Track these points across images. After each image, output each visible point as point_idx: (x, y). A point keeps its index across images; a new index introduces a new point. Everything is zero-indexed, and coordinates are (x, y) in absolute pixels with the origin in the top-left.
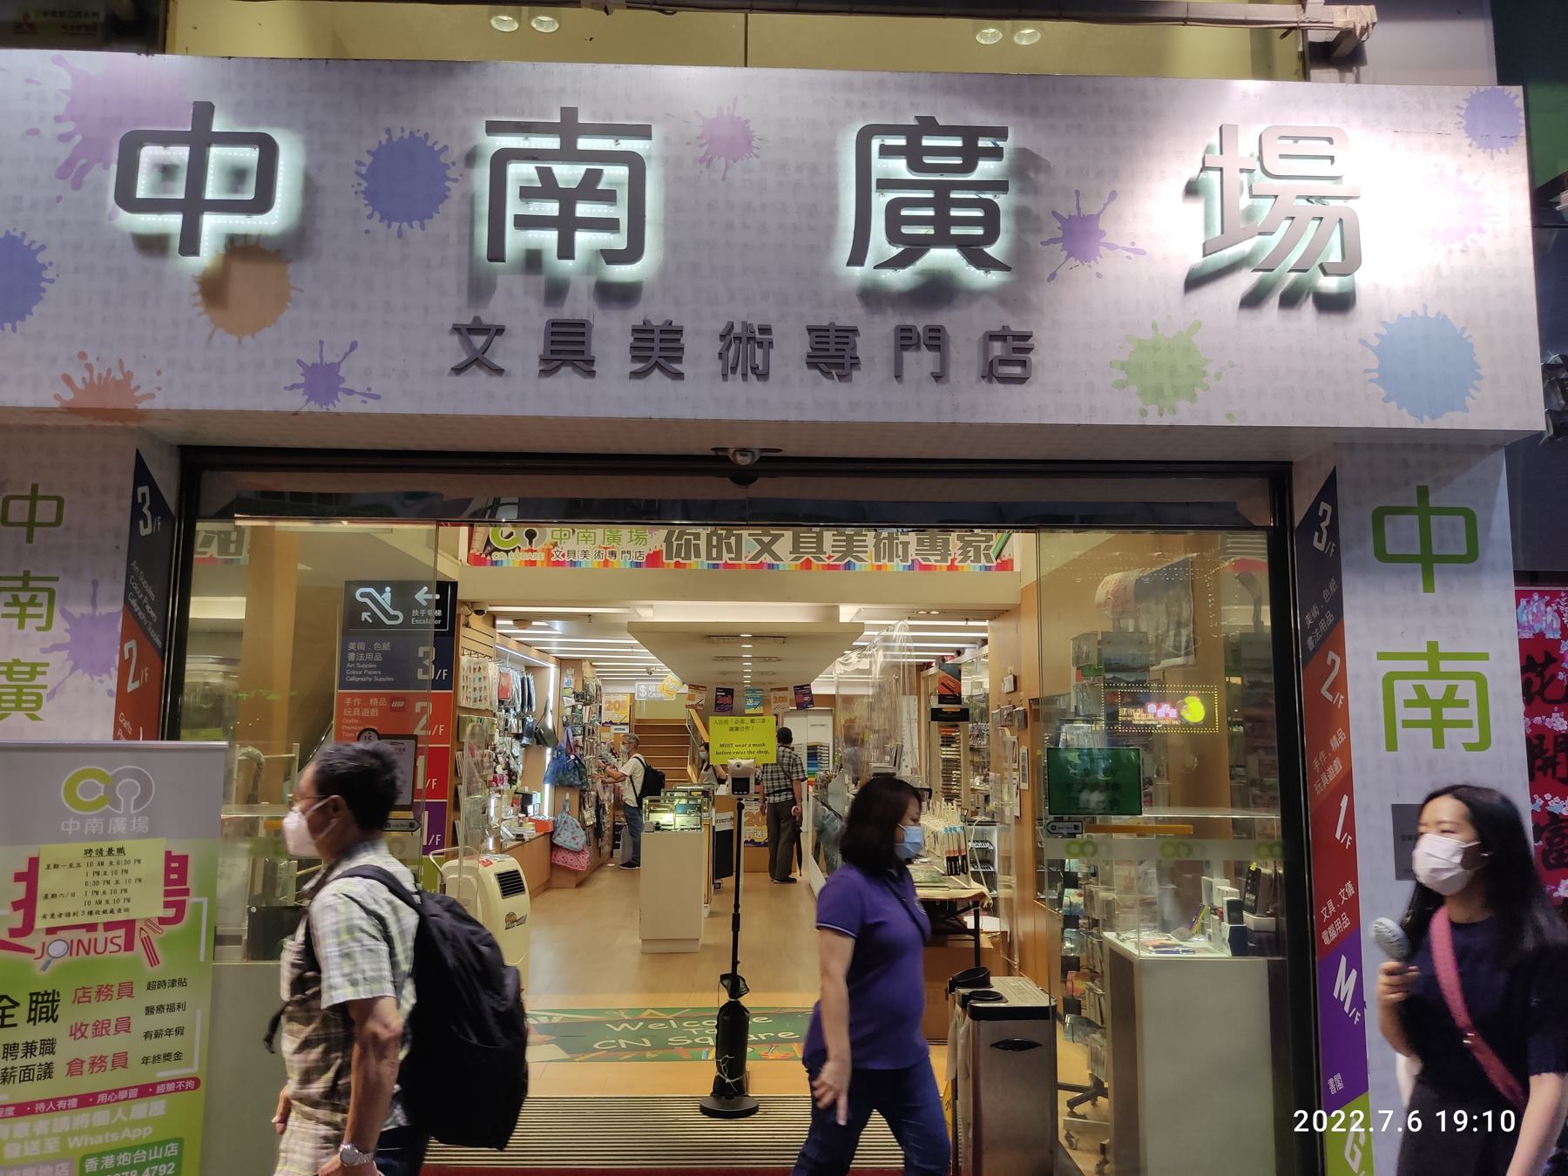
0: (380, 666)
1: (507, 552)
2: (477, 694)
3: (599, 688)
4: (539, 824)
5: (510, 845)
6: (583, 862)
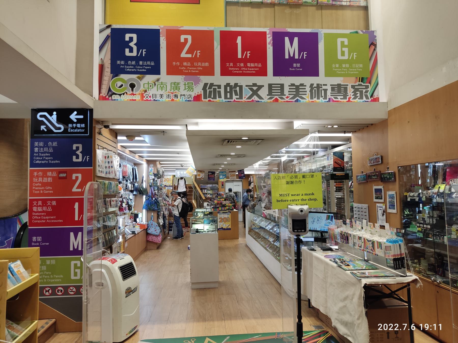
0: (52, 154)
1: (120, 95)
2: (108, 170)
3: (163, 172)
4: (141, 226)
5: (129, 236)
6: (160, 238)
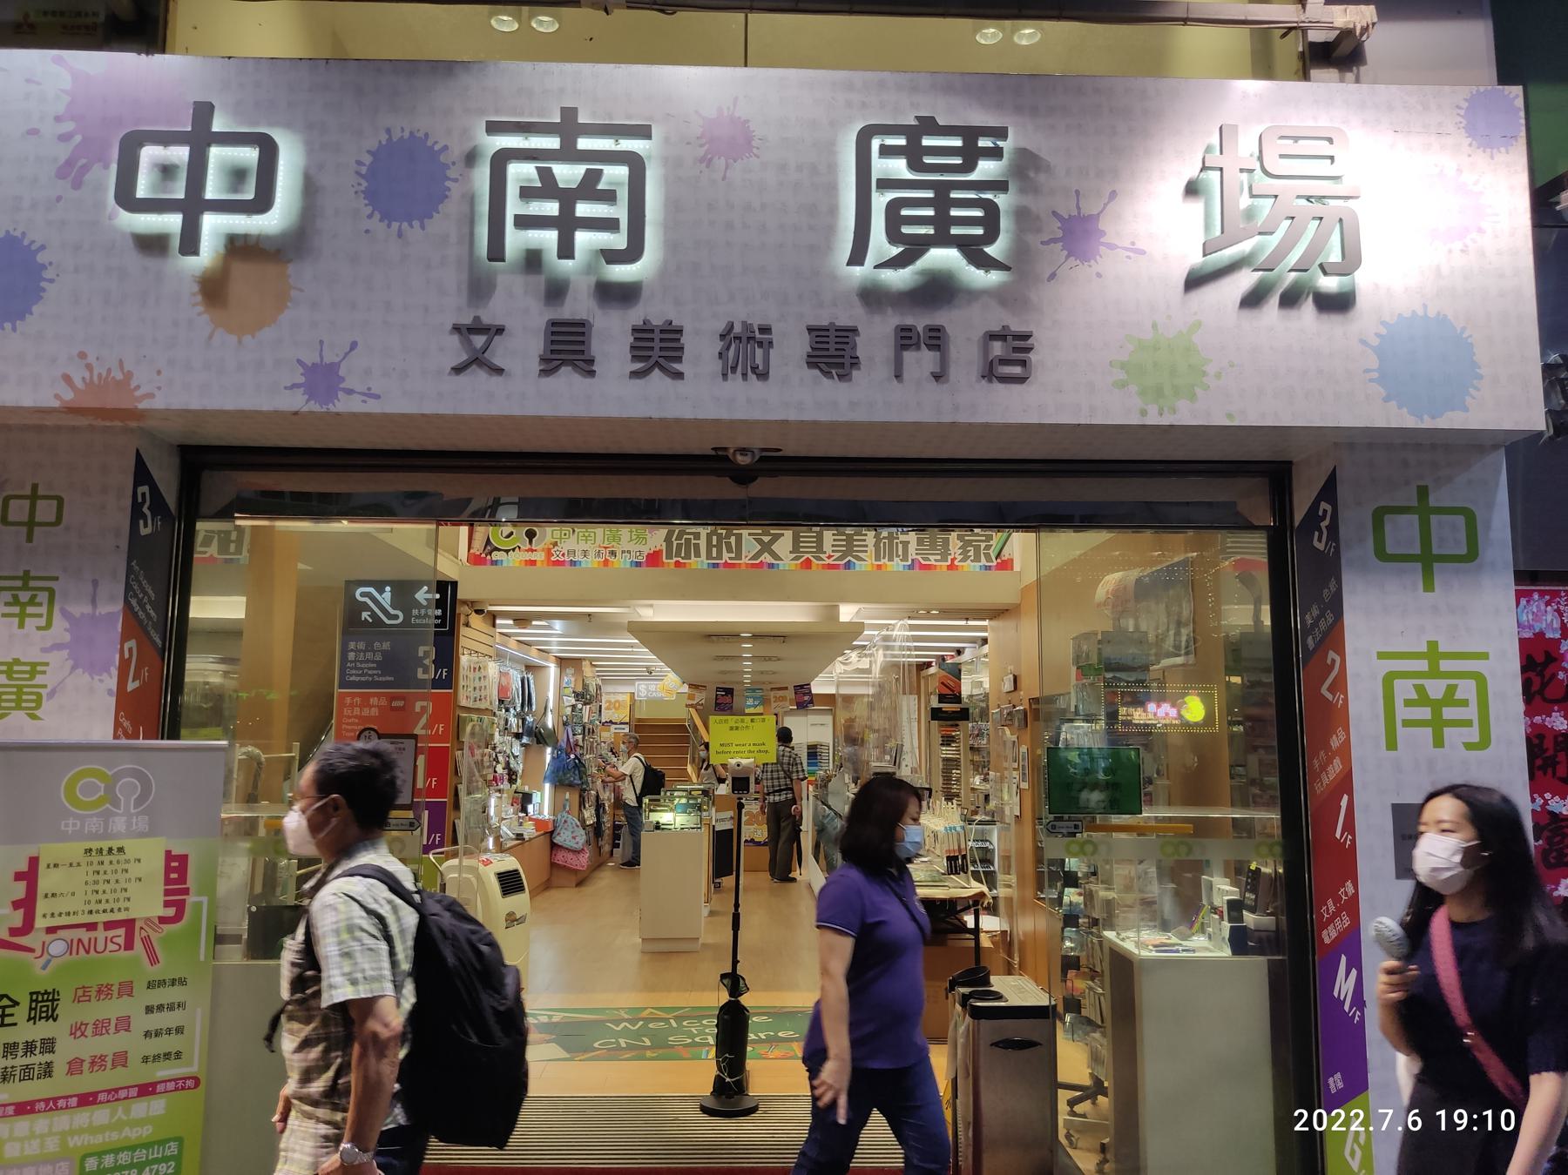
0: (380, 665)
1: (507, 551)
2: (477, 694)
3: (599, 688)
4: (539, 824)
5: (510, 844)
6: (583, 861)
